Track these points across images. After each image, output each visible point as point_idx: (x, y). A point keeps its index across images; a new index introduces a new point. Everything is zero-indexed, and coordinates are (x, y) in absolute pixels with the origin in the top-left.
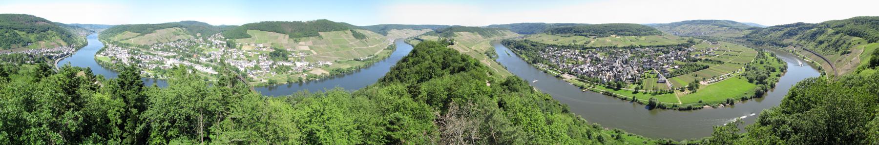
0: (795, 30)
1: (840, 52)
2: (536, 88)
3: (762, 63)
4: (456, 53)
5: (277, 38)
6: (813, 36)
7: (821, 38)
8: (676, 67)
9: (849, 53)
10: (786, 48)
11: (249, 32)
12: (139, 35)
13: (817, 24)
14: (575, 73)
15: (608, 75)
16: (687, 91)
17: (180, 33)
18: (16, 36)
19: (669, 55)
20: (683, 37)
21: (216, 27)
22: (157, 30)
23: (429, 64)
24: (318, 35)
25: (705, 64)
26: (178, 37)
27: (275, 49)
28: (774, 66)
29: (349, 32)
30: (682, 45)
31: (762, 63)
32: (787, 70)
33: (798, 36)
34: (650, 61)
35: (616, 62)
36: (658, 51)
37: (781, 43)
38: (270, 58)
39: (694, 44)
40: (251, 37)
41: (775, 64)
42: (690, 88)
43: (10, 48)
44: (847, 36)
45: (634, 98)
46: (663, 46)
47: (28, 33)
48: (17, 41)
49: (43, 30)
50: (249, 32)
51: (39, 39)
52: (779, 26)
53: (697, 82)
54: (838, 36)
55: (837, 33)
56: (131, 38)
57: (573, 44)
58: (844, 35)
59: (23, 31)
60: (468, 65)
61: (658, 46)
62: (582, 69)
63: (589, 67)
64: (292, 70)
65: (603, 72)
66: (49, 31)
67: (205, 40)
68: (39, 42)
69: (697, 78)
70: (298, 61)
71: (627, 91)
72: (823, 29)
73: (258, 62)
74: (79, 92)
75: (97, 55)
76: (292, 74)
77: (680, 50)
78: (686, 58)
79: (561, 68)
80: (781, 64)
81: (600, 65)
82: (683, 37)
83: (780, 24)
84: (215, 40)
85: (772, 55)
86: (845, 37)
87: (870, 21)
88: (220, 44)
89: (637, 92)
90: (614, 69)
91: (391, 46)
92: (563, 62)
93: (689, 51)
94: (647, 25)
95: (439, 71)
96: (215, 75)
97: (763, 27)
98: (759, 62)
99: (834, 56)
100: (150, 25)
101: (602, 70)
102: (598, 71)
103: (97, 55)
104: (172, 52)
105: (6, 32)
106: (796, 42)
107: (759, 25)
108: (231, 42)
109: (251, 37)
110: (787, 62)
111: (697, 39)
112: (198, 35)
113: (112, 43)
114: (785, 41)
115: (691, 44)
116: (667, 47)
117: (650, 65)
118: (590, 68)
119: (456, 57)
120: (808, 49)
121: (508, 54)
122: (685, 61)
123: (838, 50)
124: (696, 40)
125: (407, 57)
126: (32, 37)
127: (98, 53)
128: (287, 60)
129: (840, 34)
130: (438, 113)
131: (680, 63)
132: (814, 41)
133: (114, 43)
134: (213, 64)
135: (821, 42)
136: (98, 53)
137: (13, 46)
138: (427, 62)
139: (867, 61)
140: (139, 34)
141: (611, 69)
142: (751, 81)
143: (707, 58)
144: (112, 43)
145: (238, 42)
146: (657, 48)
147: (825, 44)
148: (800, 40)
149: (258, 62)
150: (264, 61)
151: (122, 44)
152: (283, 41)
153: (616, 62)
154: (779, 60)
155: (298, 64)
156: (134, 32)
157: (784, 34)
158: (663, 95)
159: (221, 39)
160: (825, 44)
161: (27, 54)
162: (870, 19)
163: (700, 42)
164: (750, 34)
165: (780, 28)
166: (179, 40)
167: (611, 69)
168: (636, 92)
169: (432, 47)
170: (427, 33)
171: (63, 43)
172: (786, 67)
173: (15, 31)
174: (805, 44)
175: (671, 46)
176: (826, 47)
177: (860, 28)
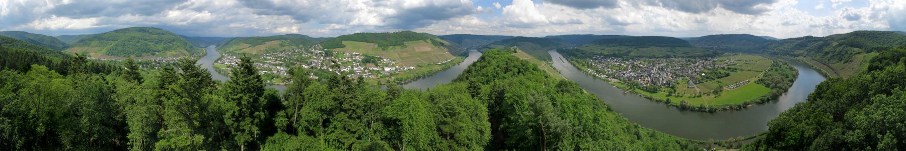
0: (806, 43)
1: (843, 61)
2: (586, 89)
3: (776, 70)
4: (517, 59)
5: (299, 29)
6: (820, 48)
7: (827, 49)
8: (703, 74)
9: (851, 61)
10: (798, 58)
11: (344, 42)
12: (250, 47)
14: (618, 78)
15: (646, 80)
16: (713, 96)
17: (285, 44)
18: (146, 46)
21: (316, 39)
22: (266, 42)
23: (495, 69)
24: (403, 44)
25: (727, 72)
26: (283, 49)
27: (366, 56)
29: (428, 41)
32: (799, 76)
33: (808, 48)
34: (682, 69)
35: (653, 69)
36: (689, 61)
37: (792, 53)
38: (361, 63)
40: (345, 46)
41: (788, 72)
42: (716, 92)
43: (141, 56)
44: (849, 48)
45: (668, 100)
47: (157, 43)
48: (148, 51)
49: (169, 41)
50: (344, 42)
51: (166, 49)
53: (721, 87)
54: (841, 48)
55: (840, 45)
56: (243, 49)
57: (617, 53)
58: (847, 47)
59: (152, 42)
60: (527, 69)
62: (624, 74)
63: (631, 72)
64: (381, 74)
65: (642, 77)
66: (175, 43)
67: (307, 50)
68: (166, 52)
69: (721, 85)
70: (386, 66)
71: (661, 95)
72: (828, 42)
73: (352, 67)
74: (892, 139)
75: (215, 64)
76: (381, 77)
79: (606, 73)
81: (640, 71)
84: (315, 50)
85: (785, 64)
86: (847, 49)
87: (868, 35)
88: (320, 53)
89: (671, 95)
90: (652, 75)
91: (465, 53)
92: (609, 68)
93: (713, 61)
95: (502, 74)
96: (316, 79)
98: (774, 70)
99: (837, 65)
100: (260, 37)
101: (642, 76)
102: (637, 76)
103: (215, 64)
104: (279, 60)
105: (138, 43)
108: (329, 51)
109: (345, 46)
110: (798, 70)
112: (301, 46)
113: (228, 53)
114: (797, 52)
117: (683, 72)
118: (631, 74)
119: (516, 63)
120: (816, 59)
122: (711, 70)
123: (842, 59)
125: (476, 62)
126: (160, 47)
127: (216, 62)
128: (377, 66)
129: (843, 46)
130: (440, 105)
132: (821, 52)
133: (229, 53)
134: (314, 70)
135: (827, 53)
136: (216, 62)
137: (144, 54)
138: (492, 67)
139: (866, 67)
140: (249, 45)
141: (649, 75)
142: (768, 86)
143: (729, 67)
144: (228, 53)
145: (335, 52)
147: (831, 54)
148: (809, 51)
149: (352, 67)
150: (357, 66)
151: (237, 54)
152: (370, 49)
153: (653, 69)
154: (792, 69)
155: (387, 69)
156: (247, 43)
157: (796, 46)
159: (320, 50)
160: (831, 54)
161: (155, 61)
162: (868, 33)
165: (792, 41)
166: (285, 51)
167: (649, 75)
168: (670, 95)
169: (498, 54)
170: (495, 42)
171: (186, 53)
172: (797, 74)
173: (146, 41)
174: (813, 54)
176: (831, 57)
177: (860, 40)
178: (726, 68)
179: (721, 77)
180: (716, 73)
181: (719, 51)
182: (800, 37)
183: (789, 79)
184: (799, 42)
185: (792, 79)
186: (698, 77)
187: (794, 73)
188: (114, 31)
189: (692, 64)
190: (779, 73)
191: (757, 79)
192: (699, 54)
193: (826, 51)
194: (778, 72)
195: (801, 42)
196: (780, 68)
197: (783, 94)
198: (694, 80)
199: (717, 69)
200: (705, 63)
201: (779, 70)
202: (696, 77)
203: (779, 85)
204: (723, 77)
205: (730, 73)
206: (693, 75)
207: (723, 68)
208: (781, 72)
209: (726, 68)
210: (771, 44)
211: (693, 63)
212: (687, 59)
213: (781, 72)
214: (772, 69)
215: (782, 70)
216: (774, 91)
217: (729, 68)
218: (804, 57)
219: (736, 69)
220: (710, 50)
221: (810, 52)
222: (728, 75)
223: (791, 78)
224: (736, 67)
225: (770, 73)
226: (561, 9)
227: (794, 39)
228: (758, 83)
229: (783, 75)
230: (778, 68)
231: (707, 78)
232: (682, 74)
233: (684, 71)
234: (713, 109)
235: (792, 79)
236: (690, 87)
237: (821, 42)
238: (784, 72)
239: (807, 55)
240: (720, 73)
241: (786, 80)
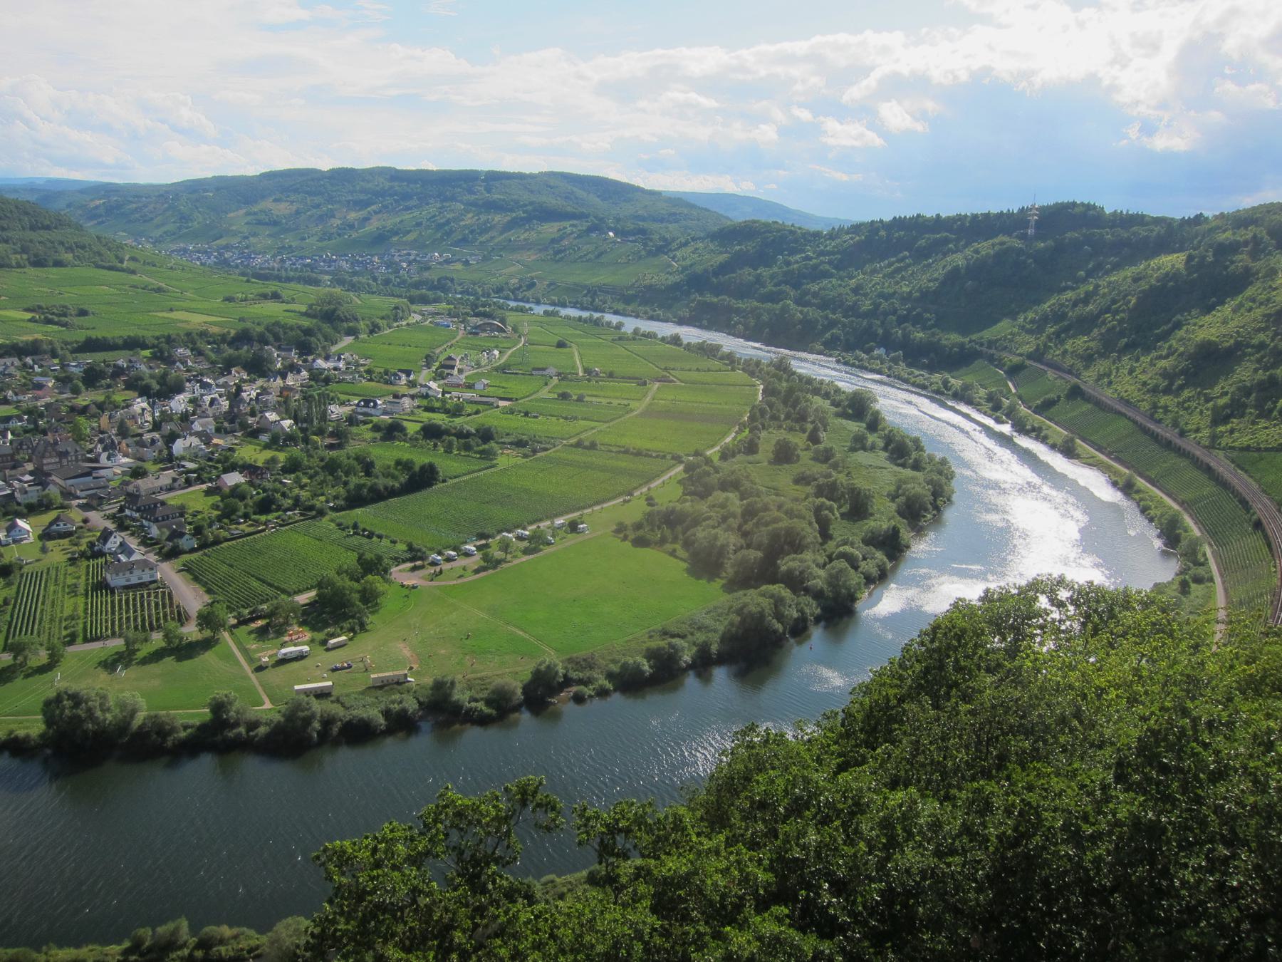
3: (784, 455)
8: (234, 479)
13: (1199, 219)
19: (179, 403)
20: (272, 287)
25: (420, 459)
28: (861, 483)
30: (275, 334)
31: (784, 455)
36: (92, 378)
39: (352, 332)
46: (132, 344)
52: (916, 226)
61: (91, 345)
77: (258, 368)
78: (296, 419)
80: (908, 472)
82: (272, 287)
83: (929, 213)
93: (316, 376)
94: (15, 190)
97: (813, 228)
106: (1029, 344)
107: (786, 210)
111: (376, 300)
115: (327, 328)
116: (162, 352)
121: (171, 310)
122: (291, 438)
124: (362, 303)
131: (251, 453)
143: (439, 419)
146: (89, 359)
158: (225, 545)
160: (1246, 373)
163: (396, 315)
164: (723, 269)
175: (192, 339)
178: (412, 428)
179: (377, 496)
180: (331, 467)
181: (357, 302)
182: (642, 185)
183: (871, 524)
184: (986, 248)
185: (895, 533)
186: (196, 500)
187: (918, 484)
188: (713, 236)
189: (140, 404)
190: (801, 480)
191: (635, 510)
192: (196, 320)
193: (1201, 335)
194: (795, 469)
195: (1001, 256)
196: (814, 439)
197: (817, 634)
198: (154, 531)
199: (340, 438)
200: (250, 393)
201: (805, 457)
202: (173, 499)
203: (787, 564)
204: (393, 493)
205: (448, 464)
206: (144, 484)
207: (392, 432)
208: (818, 469)
209: (412, 428)
210: (762, 258)
211: (145, 392)
212: (75, 369)
213: (818, 469)
214: (751, 448)
215: (826, 457)
216: (756, 599)
217: (431, 432)
218: (1014, 371)
219: (486, 435)
220: (288, 290)
221: (1059, 337)
222: (422, 479)
223: (883, 517)
224: (490, 419)
225: (737, 464)
226: (556, 339)
227: (938, 223)
228: (640, 542)
229: (829, 491)
230: (799, 440)
231: (265, 506)
232: (34, 494)
233: (50, 462)
234: (308, 721)
235: (895, 533)
236: (115, 580)
237: (1173, 261)
238: (841, 478)
239: (1037, 356)
240: (368, 468)
241: (848, 537)
